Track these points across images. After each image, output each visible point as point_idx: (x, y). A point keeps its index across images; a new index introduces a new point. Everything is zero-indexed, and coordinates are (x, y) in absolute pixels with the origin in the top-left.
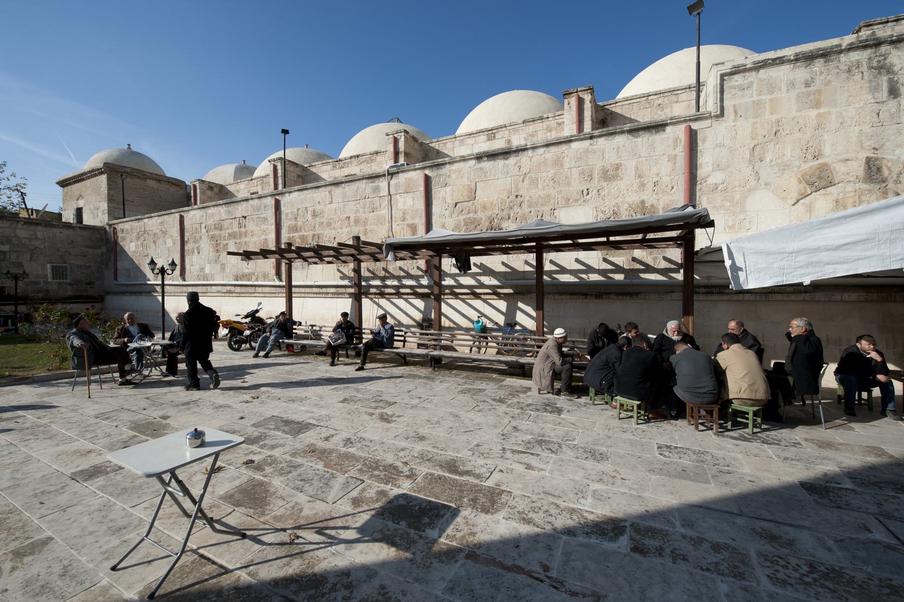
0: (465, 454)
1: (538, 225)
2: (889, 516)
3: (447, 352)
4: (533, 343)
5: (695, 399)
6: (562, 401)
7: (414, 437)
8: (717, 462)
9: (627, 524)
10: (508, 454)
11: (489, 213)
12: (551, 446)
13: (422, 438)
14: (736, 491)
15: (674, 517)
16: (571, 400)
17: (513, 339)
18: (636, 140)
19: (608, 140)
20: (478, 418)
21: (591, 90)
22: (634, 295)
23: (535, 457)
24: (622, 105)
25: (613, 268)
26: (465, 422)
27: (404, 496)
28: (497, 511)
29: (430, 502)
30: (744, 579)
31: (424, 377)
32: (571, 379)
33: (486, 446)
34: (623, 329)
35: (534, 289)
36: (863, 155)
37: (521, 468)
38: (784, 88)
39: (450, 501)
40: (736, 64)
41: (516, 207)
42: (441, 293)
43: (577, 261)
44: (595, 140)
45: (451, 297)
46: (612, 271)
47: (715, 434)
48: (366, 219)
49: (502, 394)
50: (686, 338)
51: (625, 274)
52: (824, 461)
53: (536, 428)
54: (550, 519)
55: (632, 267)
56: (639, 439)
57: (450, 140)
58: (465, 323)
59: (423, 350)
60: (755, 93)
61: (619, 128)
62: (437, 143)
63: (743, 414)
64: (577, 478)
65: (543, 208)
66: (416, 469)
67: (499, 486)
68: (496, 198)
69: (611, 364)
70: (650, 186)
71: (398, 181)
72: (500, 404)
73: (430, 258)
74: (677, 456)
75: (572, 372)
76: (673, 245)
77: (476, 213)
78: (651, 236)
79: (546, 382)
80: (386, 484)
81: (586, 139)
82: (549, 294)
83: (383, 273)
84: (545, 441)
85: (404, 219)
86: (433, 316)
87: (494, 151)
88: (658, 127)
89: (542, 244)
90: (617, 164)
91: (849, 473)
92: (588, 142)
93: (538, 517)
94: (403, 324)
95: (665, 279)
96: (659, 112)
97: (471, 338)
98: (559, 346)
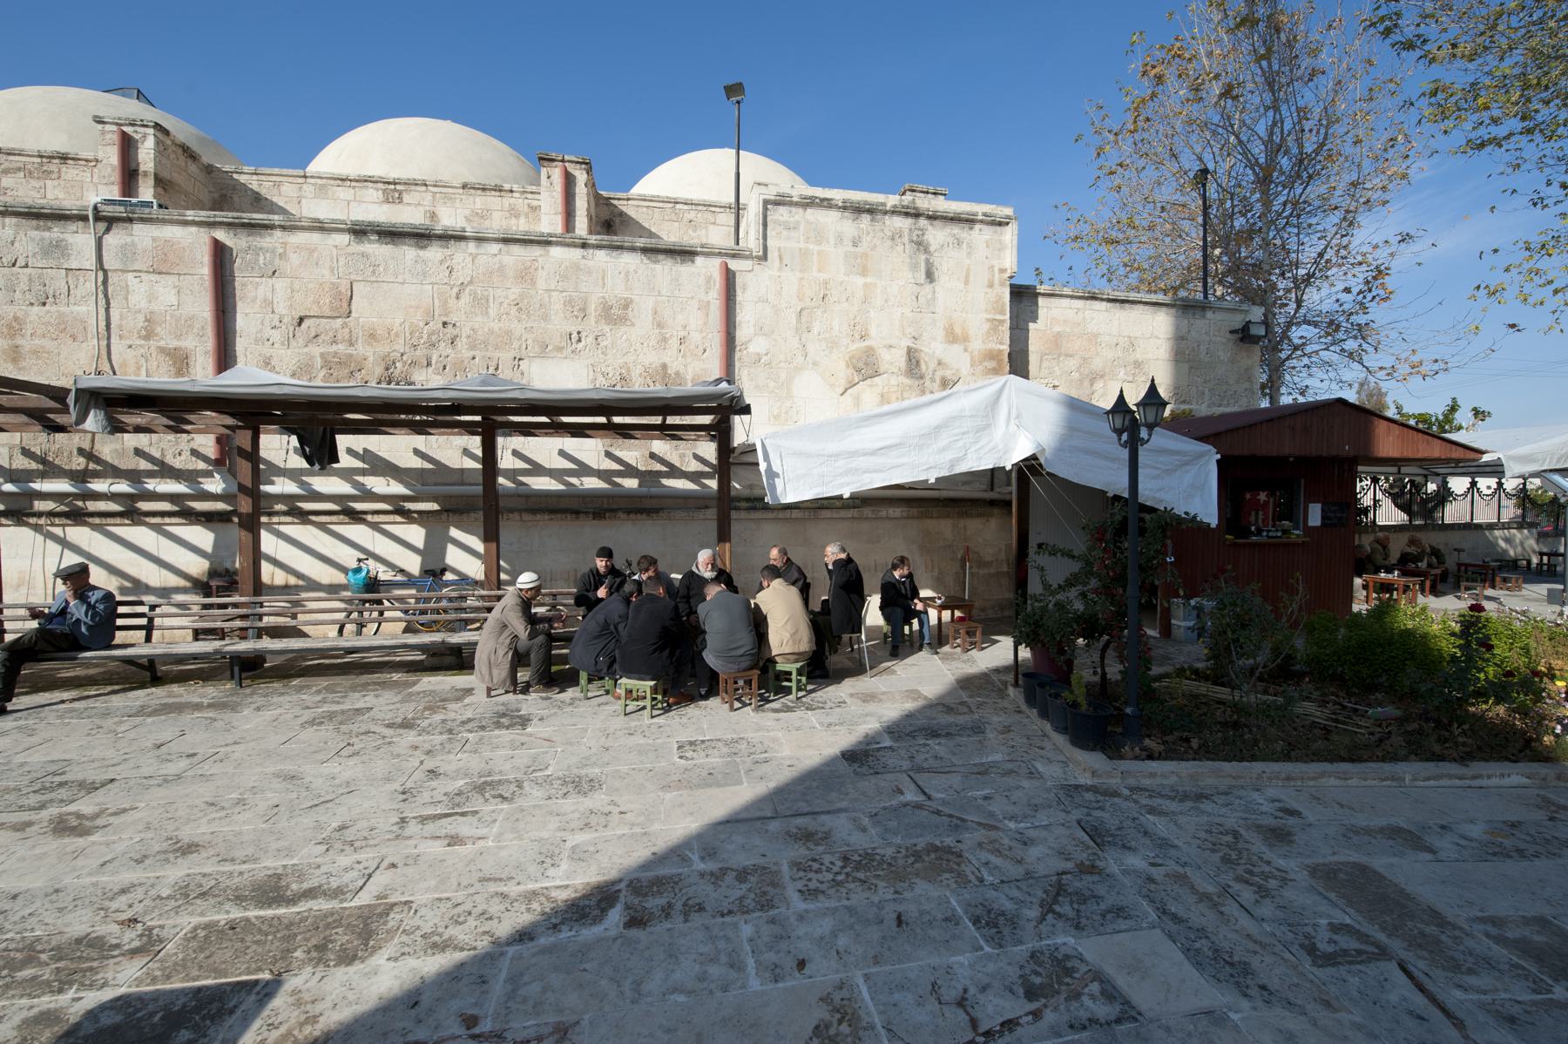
0: (309, 853)
1: (484, 383)
2: (920, 770)
3: (276, 640)
4: (477, 604)
6: (532, 703)
7: (165, 852)
8: (753, 750)
9: (622, 885)
10: (413, 828)
11: (383, 348)
12: (503, 790)
13: (189, 849)
14: (772, 785)
15: (691, 850)
16: (547, 698)
17: (439, 600)
18: (652, 266)
20: (348, 770)
21: (588, 166)
23: (469, 819)
26: (313, 786)
27: (122, 1004)
28: (375, 949)
29: (199, 990)
30: (773, 907)
31: (210, 706)
32: (549, 660)
33: (363, 824)
34: (634, 567)
35: (481, 503)
36: (906, 343)
37: (437, 848)
38: (832, 241)
39: (260, 969)
41: (443, 344)
42: (257, 512)
43: (562, 453)
44: (591, 251)
45: (288, 519)
48: (16, 319)
49: (408, 710)
50: (723, 577)
53: (474, 763)
54: (487, 926)
56: (651, 742)
57: (291, 179)
58: (326, 575)
59: (207, 643)
60: (802, 238)
61: (627, 240)
62: (255, 177)
63: (787, 675)
64: (545, 835)
65: (497, 354)
66: (162, 927)
67: (385, 897)
68: (398, 321)
69: (612, 627)
70: (674, 342)
71: (129, 239)
72: (402, 731)
73: (228, 432)
74: (703, 754)
75: (550, 648)
77: (351, 345)
78: (671, 420)
79: (501, 672)
80: (60, 991)
81: (574, 245)
82: (511, 511)
83: (79, 463)
84: (490, 784)
85: (149, 335)
86: (237, 565)
87: (394, 225)
88: (684, 254)
89: (494, 421)
90: (625, 299)
91: (888, 727)
92: (578, 252)
93: (460, 934)
94: (147, 586)
95: (696, 487)
96: (690, 232)
97: (342, 605)
98: (526, 604)
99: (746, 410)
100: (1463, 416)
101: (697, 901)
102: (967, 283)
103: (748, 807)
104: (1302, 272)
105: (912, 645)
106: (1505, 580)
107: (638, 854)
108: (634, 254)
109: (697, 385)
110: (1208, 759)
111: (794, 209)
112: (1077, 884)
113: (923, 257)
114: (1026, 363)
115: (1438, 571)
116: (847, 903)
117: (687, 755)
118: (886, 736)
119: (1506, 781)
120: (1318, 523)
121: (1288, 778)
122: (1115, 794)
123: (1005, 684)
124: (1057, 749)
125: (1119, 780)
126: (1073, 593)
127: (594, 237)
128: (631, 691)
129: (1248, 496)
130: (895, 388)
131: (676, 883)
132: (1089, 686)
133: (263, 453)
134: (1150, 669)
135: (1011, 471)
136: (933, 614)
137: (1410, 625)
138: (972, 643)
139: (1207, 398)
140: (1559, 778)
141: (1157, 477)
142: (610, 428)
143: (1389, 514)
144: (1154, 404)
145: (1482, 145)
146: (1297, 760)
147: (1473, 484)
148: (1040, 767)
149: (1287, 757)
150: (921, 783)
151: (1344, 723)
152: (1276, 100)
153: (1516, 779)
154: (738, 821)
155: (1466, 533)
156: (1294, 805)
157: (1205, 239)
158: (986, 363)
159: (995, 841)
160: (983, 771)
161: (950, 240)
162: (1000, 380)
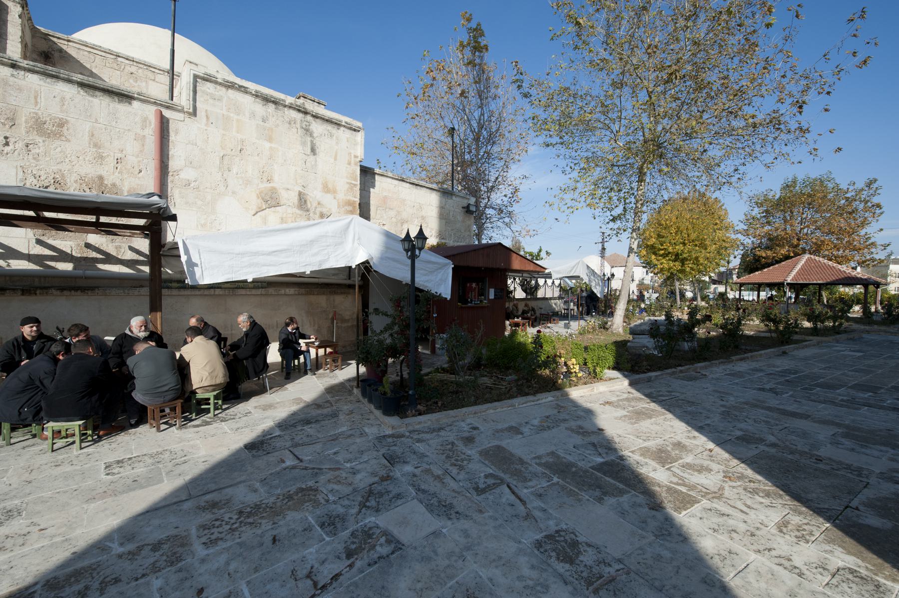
2: (296, 445)
5: (157, 399)
14: (188, 478)
18: (91, 99)
19: (45, 82)
22: (88, 290)
24: (79, 49)
25: (55, 254)
40: (209, 72)
46: (52, 258)
47: (177, 429)
51: (74, 263)
52: (265, 421)
55: (85, 255)
56: (78, 468)
61: (63, 73)
63: (206, 401)
69: (38, 383)
74: (130, 468)
76: (140, 234)
88: (124, 97)
91: (279, 423)
95: (131, 271)
96: (131, 81)
99: (174, 218)
100: (543, 254)
101: (113, 577)
102: (335, 159)
103: (165, 499)
104: (490, 184)
105: (299, 372)
106: (554, 320)
107: (58, 557)
108: (70, 86)
109: (131, 195)
111: (218, 87)
112: (380, 488)
113: (309, 139)
115: (533, 317)
116: (239, 540)
117: (114, 471)
118: (277, 429)
119: (547, 400)
121: (475, 413)
122: (403, 436)
123: (352, 387)
124: (376, 418)
125: (405, 429)
126: (386, 335)
127: (26, 62)
128: (60, 432)
130: (291, 215)
131: (95, 569)
132: (393, 383)
134: (421, 370)
136: (313, 352)
137: (522, 340)
140: (562, 396)
142: (38, 221)
143: (519, 294)
145: (548, 146)
146: (479, 404)
147: (546, 281)
148: (367, 430)
149: (475, 403)
150: (296, 453)
152: (482, 104)
153: (550, 399)
154: (156, 509)
155: (543, 301)
156: (478, 425)
157: (453, 161)
158: (346, 207)
159: (338, 476)
160: (335, 438)
161: (326, 133)
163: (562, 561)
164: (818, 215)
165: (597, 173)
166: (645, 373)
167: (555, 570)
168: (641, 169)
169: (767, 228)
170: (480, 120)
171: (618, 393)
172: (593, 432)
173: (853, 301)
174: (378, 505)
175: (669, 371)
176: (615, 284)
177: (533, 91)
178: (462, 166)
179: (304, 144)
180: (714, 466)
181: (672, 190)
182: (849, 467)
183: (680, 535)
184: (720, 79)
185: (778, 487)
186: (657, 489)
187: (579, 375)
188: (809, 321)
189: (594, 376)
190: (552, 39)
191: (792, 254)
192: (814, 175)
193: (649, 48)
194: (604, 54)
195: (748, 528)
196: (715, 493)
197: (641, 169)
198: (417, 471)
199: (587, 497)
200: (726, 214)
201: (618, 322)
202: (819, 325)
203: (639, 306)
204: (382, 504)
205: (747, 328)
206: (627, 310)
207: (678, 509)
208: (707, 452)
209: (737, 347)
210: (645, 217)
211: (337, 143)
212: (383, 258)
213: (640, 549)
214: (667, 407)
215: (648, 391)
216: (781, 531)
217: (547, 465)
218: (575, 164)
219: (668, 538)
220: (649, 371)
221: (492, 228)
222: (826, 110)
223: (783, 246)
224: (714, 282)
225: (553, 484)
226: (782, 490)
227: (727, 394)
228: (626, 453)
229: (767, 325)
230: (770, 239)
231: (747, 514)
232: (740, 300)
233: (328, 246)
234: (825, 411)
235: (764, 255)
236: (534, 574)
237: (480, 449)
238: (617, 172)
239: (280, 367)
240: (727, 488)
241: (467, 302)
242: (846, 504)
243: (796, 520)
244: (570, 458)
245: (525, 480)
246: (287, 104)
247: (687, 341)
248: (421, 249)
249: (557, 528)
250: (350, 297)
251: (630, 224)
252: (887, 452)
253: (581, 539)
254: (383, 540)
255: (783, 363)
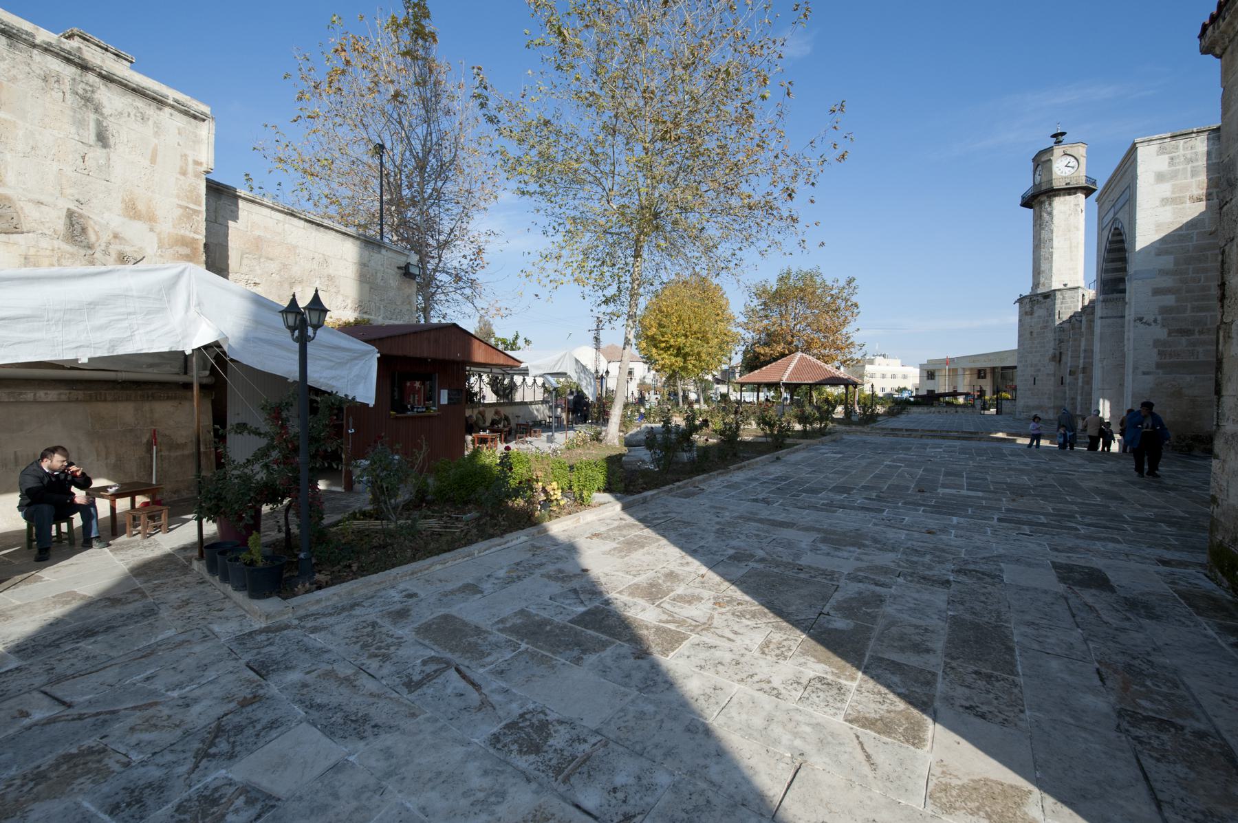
2: (60, 679)
36: (66, 204)
91: (18, 646)
100: (520, 342)
102: (153, 161)
104: (442, 238)
106: (535, 432)
110: (363, 576)
112: (237, 719)
113: (92, 117)
114: (226, 257)
115: (507, 429)
120: (446, 402)
122: (287, 627)
124: (237, 605)
125: (290, 615)
126: (257, 467)
129: (408, 384)
133: (1028, 294)
135: (192, 355)
137: (488, 461)
138: (156, 527)
139: (382, 312)
141: (331, 368)
144: (317, 310)
145: (523, 193)
147: (524, 380)
148: (216, 628)
149: (414, 559)
150: (59, 694)
151: (450, 528)
153: (524, 538)
156: (415, 590)
157: (381, 196)
158: (176, 248)
160: (149, 653)
162: (182, 265)
163: (525, 753)
164: (809, 311)
165: (586, 239)
166: (640, 492)
167: (516, 768)
168: (637, 240)
169: (766, 322)
170: (425, 140)
171: (609, 521)
172: (575, 576)
173: (836, 402)
174: (233, 747)
175: (666, 488)
176: (611, 383)
177: (503, 116)
178: (398, 206)
179: (80, 123)
180: (706, 594)
181: (671, 272)
182: (824, 573)
183: (666, 682)
184: (719, 147)
185: (763, 605)
186: (645, 632)
187: (562, 503)
188: (800, 423)
189: (581, 502)
190: (528, 46)
191: (787, 352)
192: (805, 269)
193: (644, 91)
194: (595, 88)
195: (734, 657)
196: (704, 624)
197: (637, 240)
198: (309, 679)
199: (563, 661)
200: (727, 303)
201: (613, 433)
202: (808, 427)
203: (638, 411)
204: (242, 745)
205: (745, 433)
206: (624, 416)
207: (665, 652)
208: (700, 579)
209: (735, 455)
210: (643, 302)
211: (156, 134)
212: (247, 339)
213: (622, 710)
214: (661, 532)
215: (642, 515)
216: (763, 653)
217: (514, 630)
218: (560, 224)
219: (654, 689)
220: (645, 489)
221: (446, 301)
222: (812, 201)
223: (778, 343)
224: (718, 381)
225: (521, 653)
226: (767, 608)
227: (723, 509)
228: (613, 595)
229: (763, 429)
230: (768, 335)
231: (733, 641)
232: (739, 402)
233: (130, 314)
234: (808, 517)
235: (762, 352)
236: (487, 782)
237: (416, 625)
238: (611, 241)
239: (25, 540)
240: (716, 616)
241: (405, 409)
242: (818, 611)
243: (777, 637)
244: (545, 614)
245: (483, 655)
246: (37, 41)
247: (686, 451)
248: (317, 327)
249: (521, 712)
250: (187, 404)
251: (625, 309)
252: (854, 552)
253: (552, 717)
254: (240, 802)
255: (776, 470)
